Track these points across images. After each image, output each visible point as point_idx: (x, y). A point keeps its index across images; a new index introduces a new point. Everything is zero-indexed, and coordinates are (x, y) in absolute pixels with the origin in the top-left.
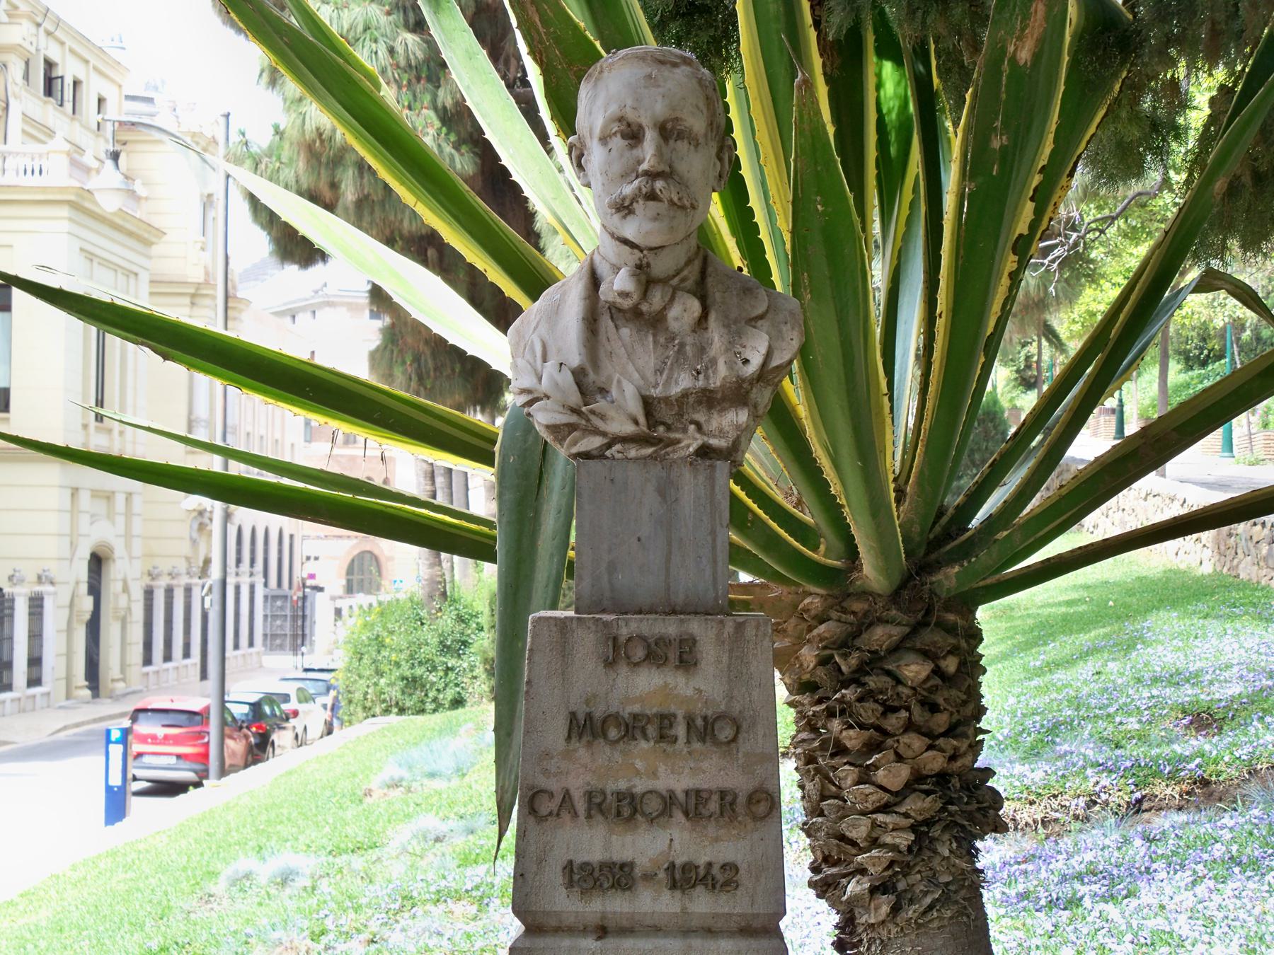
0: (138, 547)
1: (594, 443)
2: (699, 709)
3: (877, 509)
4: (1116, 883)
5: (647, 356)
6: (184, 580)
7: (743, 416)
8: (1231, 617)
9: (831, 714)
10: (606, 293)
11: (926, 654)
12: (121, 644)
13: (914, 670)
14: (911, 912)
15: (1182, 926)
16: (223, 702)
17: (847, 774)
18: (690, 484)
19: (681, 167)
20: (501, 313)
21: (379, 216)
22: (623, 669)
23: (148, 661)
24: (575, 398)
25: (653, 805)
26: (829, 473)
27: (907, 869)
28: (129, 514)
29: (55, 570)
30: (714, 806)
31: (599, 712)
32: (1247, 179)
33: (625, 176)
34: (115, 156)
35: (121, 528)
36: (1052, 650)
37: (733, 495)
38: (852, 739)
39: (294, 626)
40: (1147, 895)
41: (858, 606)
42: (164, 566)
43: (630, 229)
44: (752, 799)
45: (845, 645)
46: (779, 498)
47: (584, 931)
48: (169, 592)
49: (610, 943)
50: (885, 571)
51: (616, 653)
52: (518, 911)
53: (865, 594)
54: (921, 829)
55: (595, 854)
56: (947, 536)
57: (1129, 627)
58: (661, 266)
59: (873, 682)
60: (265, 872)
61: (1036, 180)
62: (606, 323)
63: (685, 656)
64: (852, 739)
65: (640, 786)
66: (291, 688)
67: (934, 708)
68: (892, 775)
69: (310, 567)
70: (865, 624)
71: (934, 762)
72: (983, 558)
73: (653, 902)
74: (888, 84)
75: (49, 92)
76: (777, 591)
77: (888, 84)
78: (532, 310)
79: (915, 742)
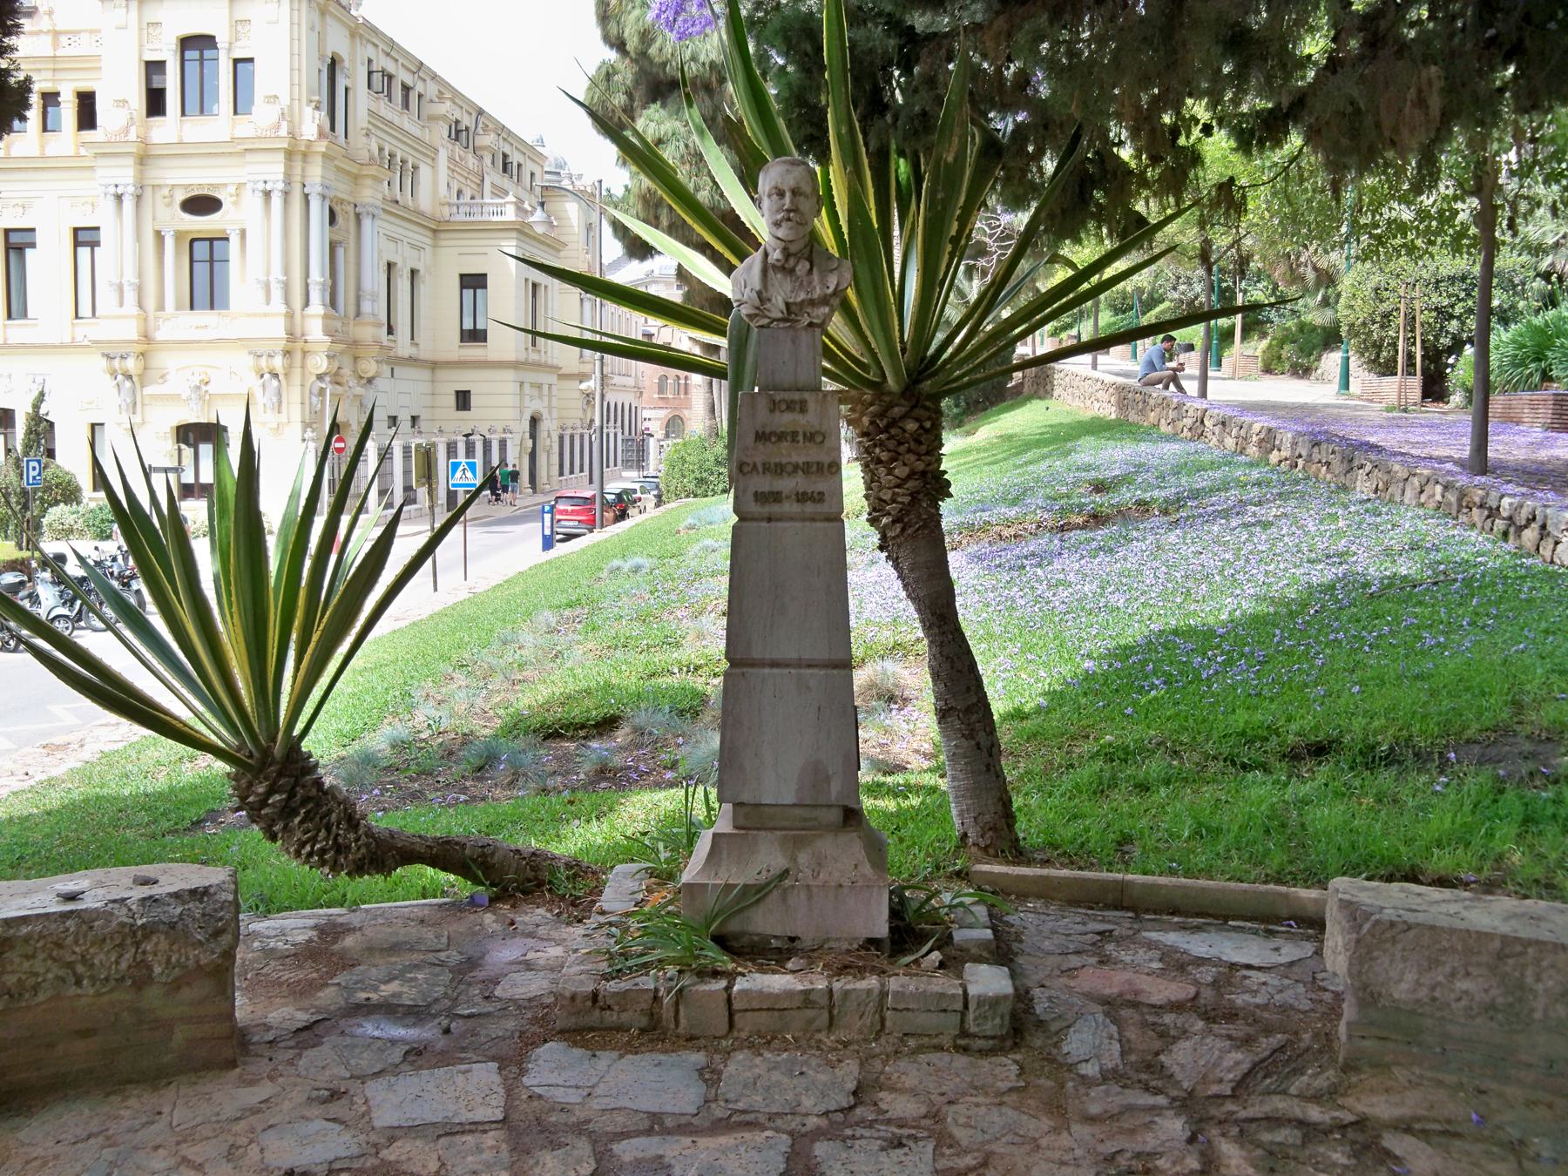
0: (555, 415)
1: (766, 321)
2: (809, 430)
3: (892, 353)
4: (1041, 559)
5: (788, 285)
6: (580, 431)
7: (827, 310)
8: (1121, 439)
9: (875, 446)
10: (770, 260)
11: (917, 420)
12: (547, 465)
13: (911, 426)
14: (910, 531)
15: (1071, 577)
16: (602, 493)
17: (882, 470)
18: (804, 337)
19: (802, 208)
20: (728, 269)
21: (677, 230)
22: (777, 413)
23: (561, 474)
24: (757, 303)
25: (790, 468)
26: (871, 339)
27: (908, 513)
28: (550, 396)
29: (513, 426)
30: (814, 468)
31: (768, 430)
32: (1058, 211)
33: (778, 211)
34: (542, 204)
35: (546, 404)
36: (1029, 456)
37: (825, 344)
38: (884, 456)
39: (637, 455)
40: (1057, 565)
41: (887, 399)
42: (569, 423)
43: (780, 233)
44: (830, 466)
45: (882, 415)
46: (853, 352)
47: (762, 519)
48: (572, 437)
49: (773, 524)
50: (897, 382)
51: (774, 406)
52: (736, 511)
53: (890, 393)
54: (914, 495)
55: (766, 489)
56: (927, 368)
57: (1069, 445)
58: (793, 248)
59: (893, 431)
60: (626, 567)
61: (958, 212)
62: (771, 271)
63: (803, 409)
64: (884, 456)
65: (784, 461)
66: (637, 486)
67: (920, 443)
68: (902, 471)
69: (646, 424)
70: (891, 406)
71: (920, 466)
72: (941, 377)
73: (790, 507)
74: (902, 167)
75: (505, 170)
76: (853, 392)
77: (902, 167)
78: (741, 267)
79: (912, 457)
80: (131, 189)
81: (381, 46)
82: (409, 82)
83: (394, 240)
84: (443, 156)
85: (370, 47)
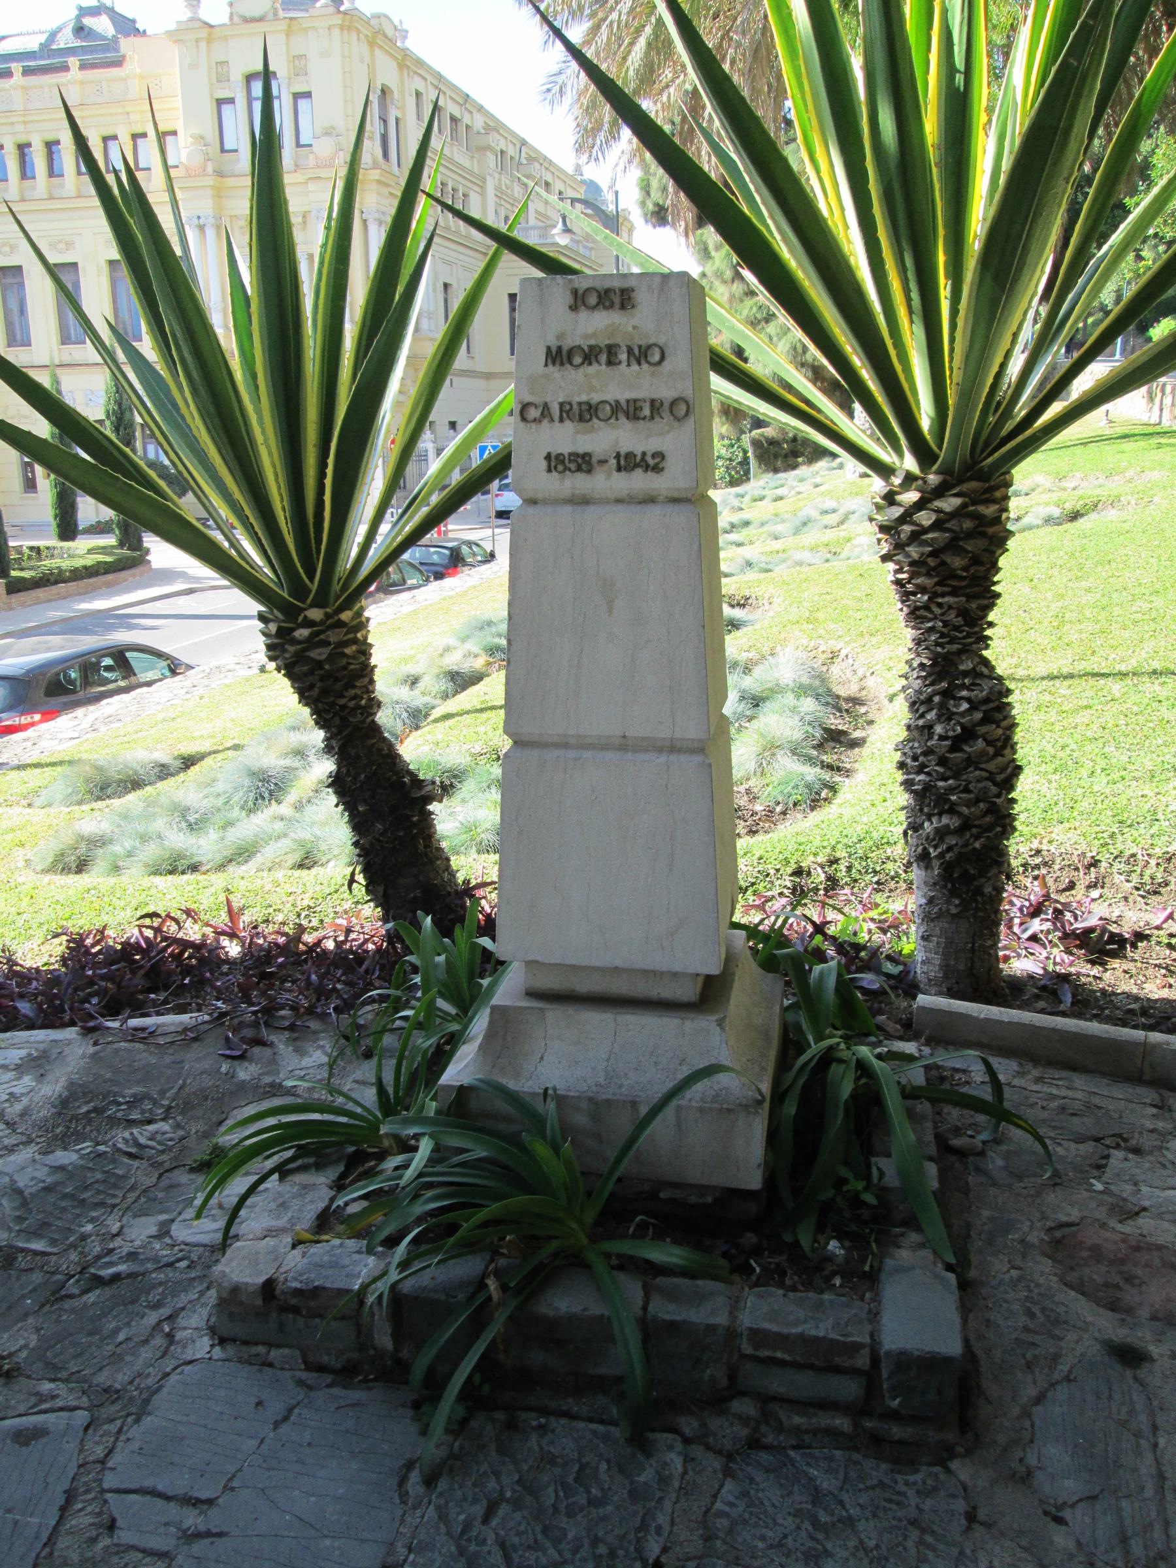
30: (647, 412)
31: (567, 344)
49: (1081, 522)
55: (566, 448)
65: (595, 398)
80: (211, 221)
81: (430, 79)
82: (458, 115)
83: (450, 263)
84: (490, 185)
85: (417, 79)
